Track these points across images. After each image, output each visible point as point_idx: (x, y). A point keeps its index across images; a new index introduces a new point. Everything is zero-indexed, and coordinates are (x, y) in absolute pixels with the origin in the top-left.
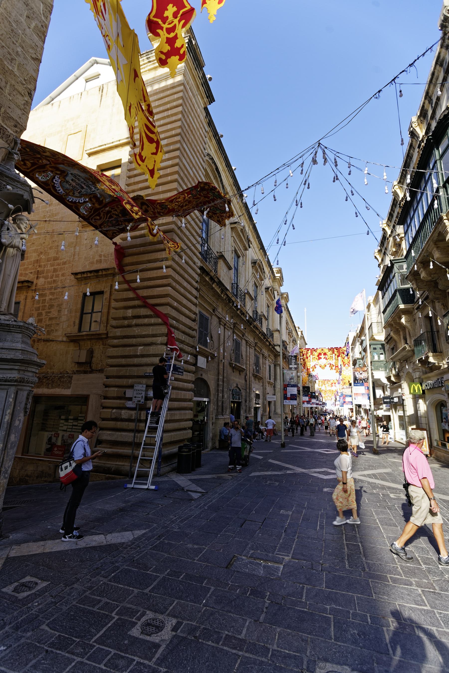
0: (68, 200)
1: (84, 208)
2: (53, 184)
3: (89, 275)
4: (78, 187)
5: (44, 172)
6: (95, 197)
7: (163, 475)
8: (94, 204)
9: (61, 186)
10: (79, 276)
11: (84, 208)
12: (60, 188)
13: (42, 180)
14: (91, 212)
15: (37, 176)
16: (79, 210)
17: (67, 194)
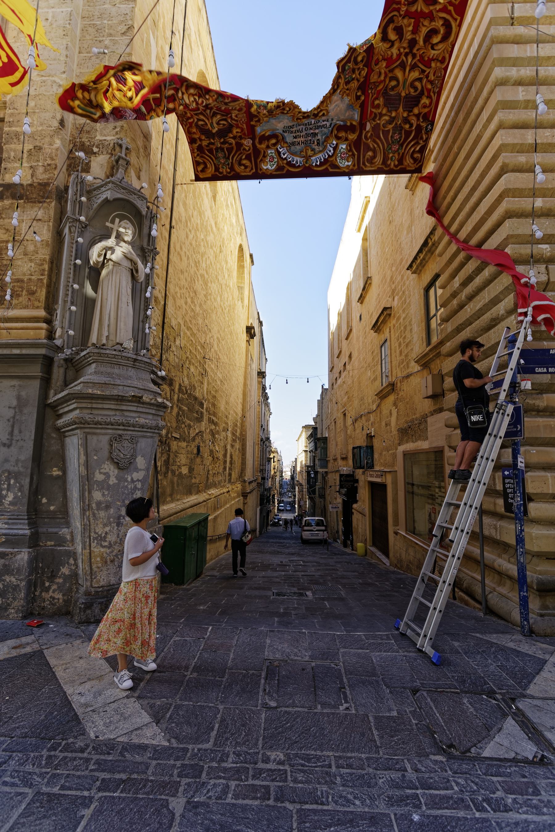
0: (316, 165)
1: (342, 158)
2: (285, 162)
3: (422, 256)
4: (310, 138)
5: (264, 156)
6: (340, 128)
7: (417, 535)
8: (346, 139)
9: (292, 154)
10: (415, 267)
11: (342, 158)
12: (296, 158)
13: (273, 168)
14: (353, 155)
15: (265, 168)
16: (338, 167)
17: (308, 158)
